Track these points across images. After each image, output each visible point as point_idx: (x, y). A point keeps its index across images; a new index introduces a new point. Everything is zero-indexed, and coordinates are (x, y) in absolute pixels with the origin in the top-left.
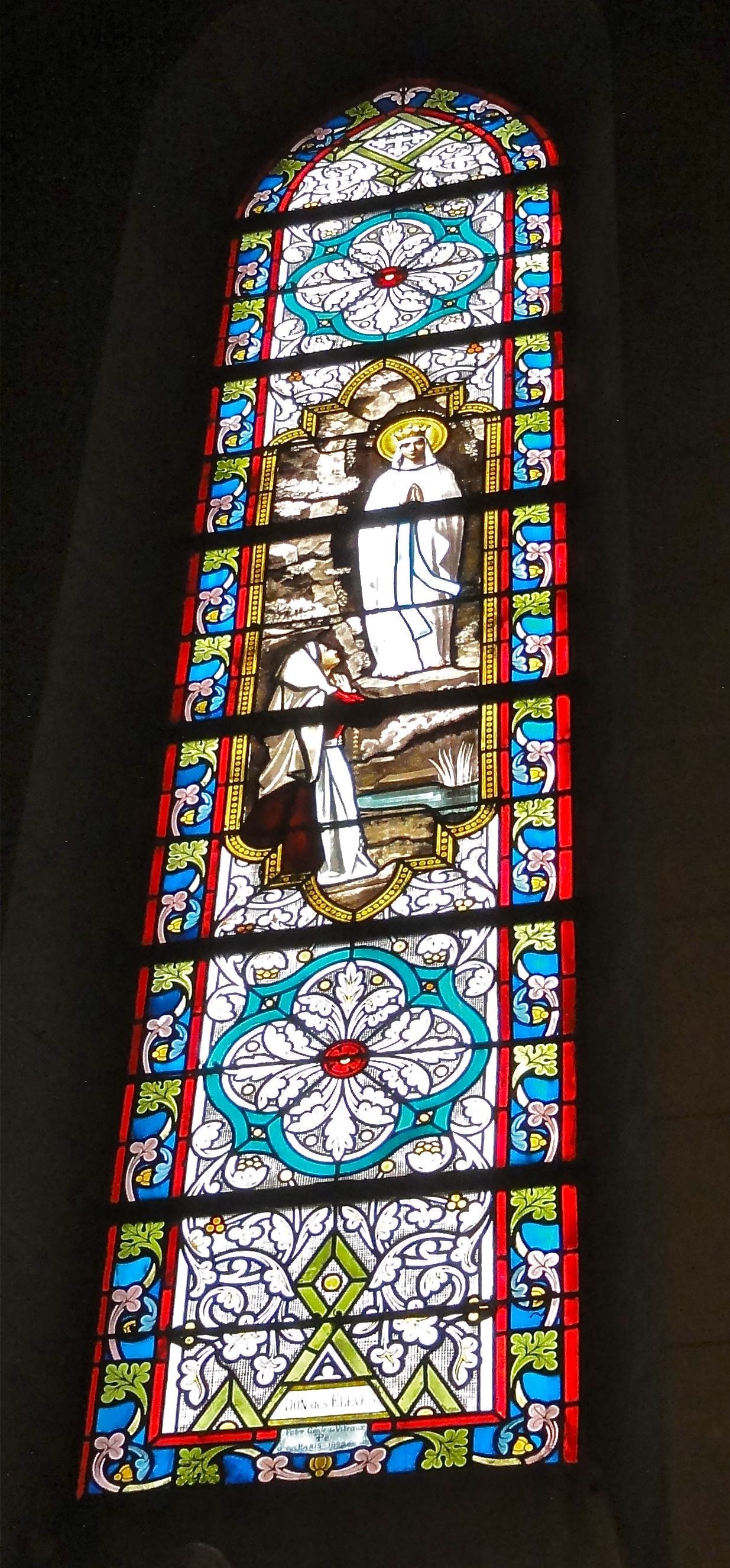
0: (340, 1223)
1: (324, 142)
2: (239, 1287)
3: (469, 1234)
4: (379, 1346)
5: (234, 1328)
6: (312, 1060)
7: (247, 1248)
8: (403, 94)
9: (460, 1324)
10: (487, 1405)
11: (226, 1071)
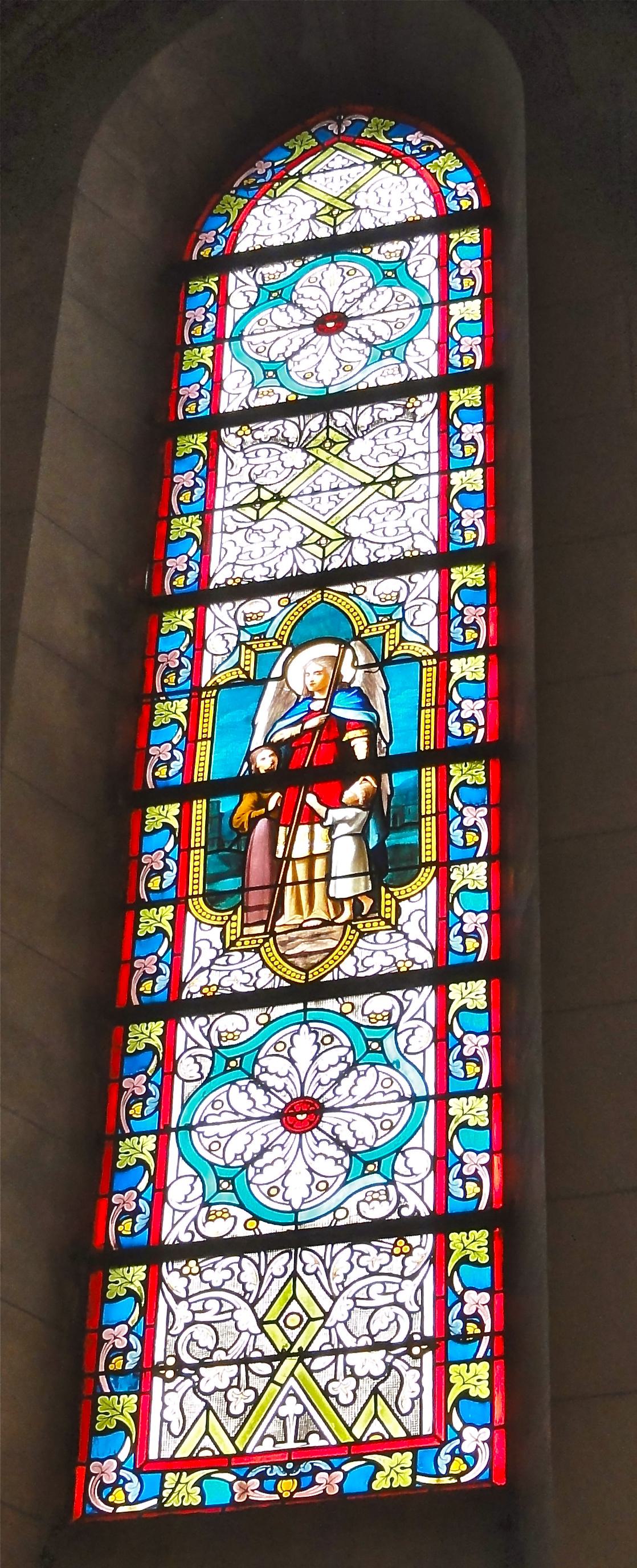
0: (300, 1265)
1: (264, 175)
4: (335, 1379)
6: (272, 1117)
7: (219, 1289)
10: (427, 1430)
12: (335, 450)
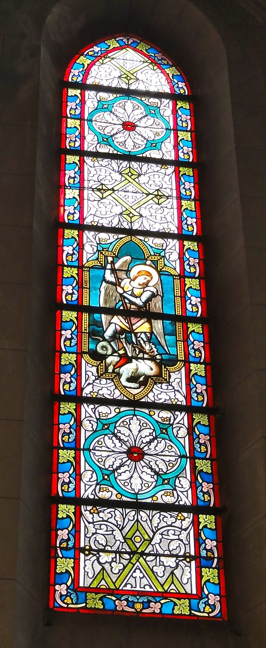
0: (139, 517)
1: (98, 53)
2: (103, 535)
3: (185, 530)
4: (156, 566)
5: (104, 551)
6: (124, 452)
7: (106, 521)
8: (128, 40)
9: (184, 561)
11: (92, 451)
12: (133, 177)
